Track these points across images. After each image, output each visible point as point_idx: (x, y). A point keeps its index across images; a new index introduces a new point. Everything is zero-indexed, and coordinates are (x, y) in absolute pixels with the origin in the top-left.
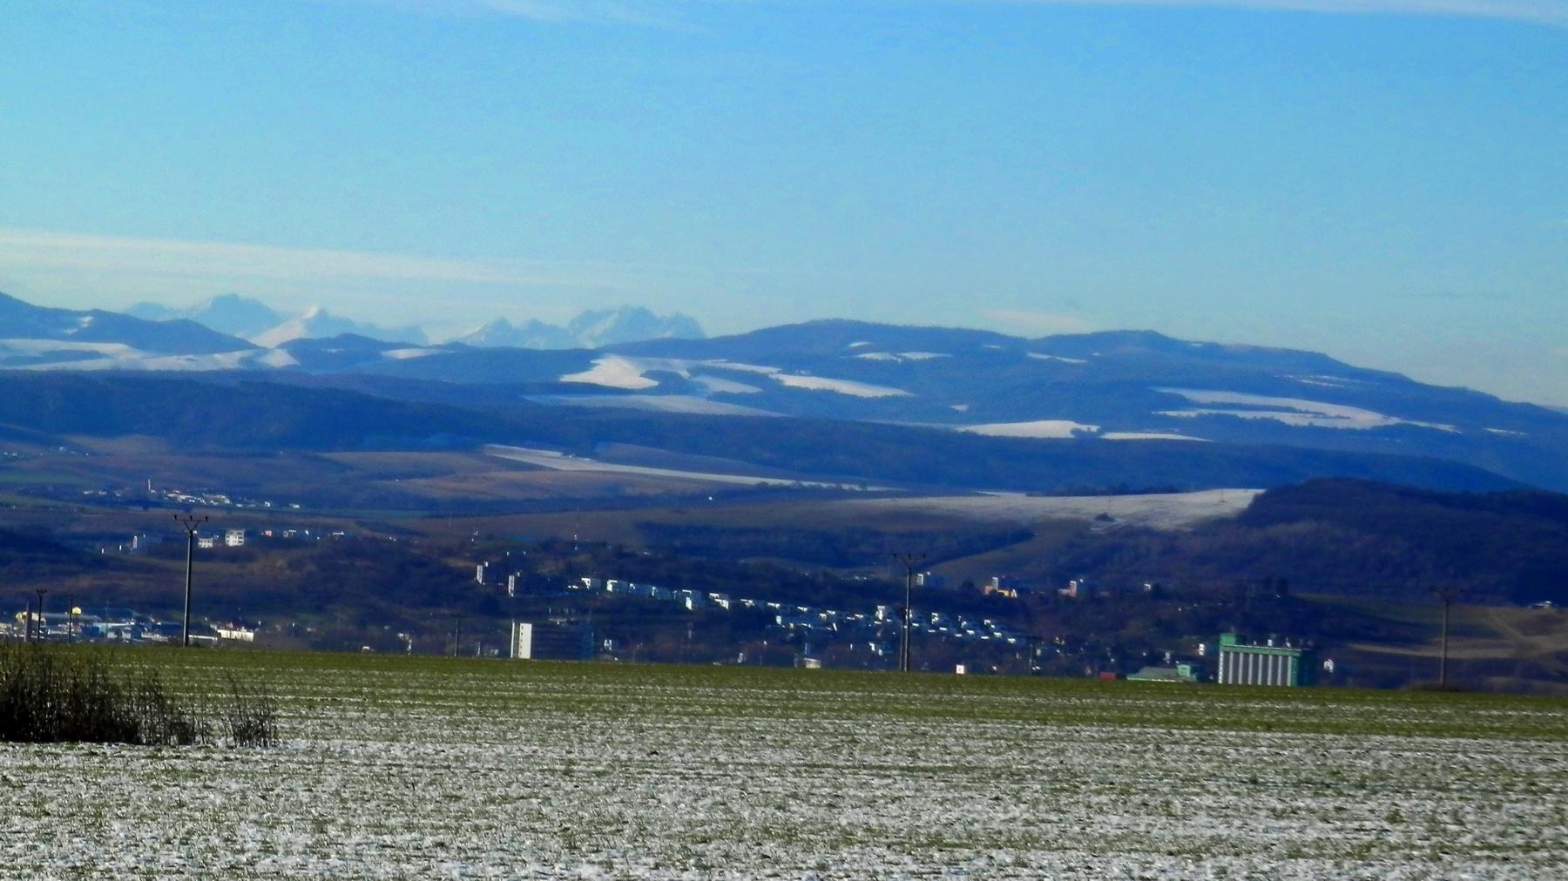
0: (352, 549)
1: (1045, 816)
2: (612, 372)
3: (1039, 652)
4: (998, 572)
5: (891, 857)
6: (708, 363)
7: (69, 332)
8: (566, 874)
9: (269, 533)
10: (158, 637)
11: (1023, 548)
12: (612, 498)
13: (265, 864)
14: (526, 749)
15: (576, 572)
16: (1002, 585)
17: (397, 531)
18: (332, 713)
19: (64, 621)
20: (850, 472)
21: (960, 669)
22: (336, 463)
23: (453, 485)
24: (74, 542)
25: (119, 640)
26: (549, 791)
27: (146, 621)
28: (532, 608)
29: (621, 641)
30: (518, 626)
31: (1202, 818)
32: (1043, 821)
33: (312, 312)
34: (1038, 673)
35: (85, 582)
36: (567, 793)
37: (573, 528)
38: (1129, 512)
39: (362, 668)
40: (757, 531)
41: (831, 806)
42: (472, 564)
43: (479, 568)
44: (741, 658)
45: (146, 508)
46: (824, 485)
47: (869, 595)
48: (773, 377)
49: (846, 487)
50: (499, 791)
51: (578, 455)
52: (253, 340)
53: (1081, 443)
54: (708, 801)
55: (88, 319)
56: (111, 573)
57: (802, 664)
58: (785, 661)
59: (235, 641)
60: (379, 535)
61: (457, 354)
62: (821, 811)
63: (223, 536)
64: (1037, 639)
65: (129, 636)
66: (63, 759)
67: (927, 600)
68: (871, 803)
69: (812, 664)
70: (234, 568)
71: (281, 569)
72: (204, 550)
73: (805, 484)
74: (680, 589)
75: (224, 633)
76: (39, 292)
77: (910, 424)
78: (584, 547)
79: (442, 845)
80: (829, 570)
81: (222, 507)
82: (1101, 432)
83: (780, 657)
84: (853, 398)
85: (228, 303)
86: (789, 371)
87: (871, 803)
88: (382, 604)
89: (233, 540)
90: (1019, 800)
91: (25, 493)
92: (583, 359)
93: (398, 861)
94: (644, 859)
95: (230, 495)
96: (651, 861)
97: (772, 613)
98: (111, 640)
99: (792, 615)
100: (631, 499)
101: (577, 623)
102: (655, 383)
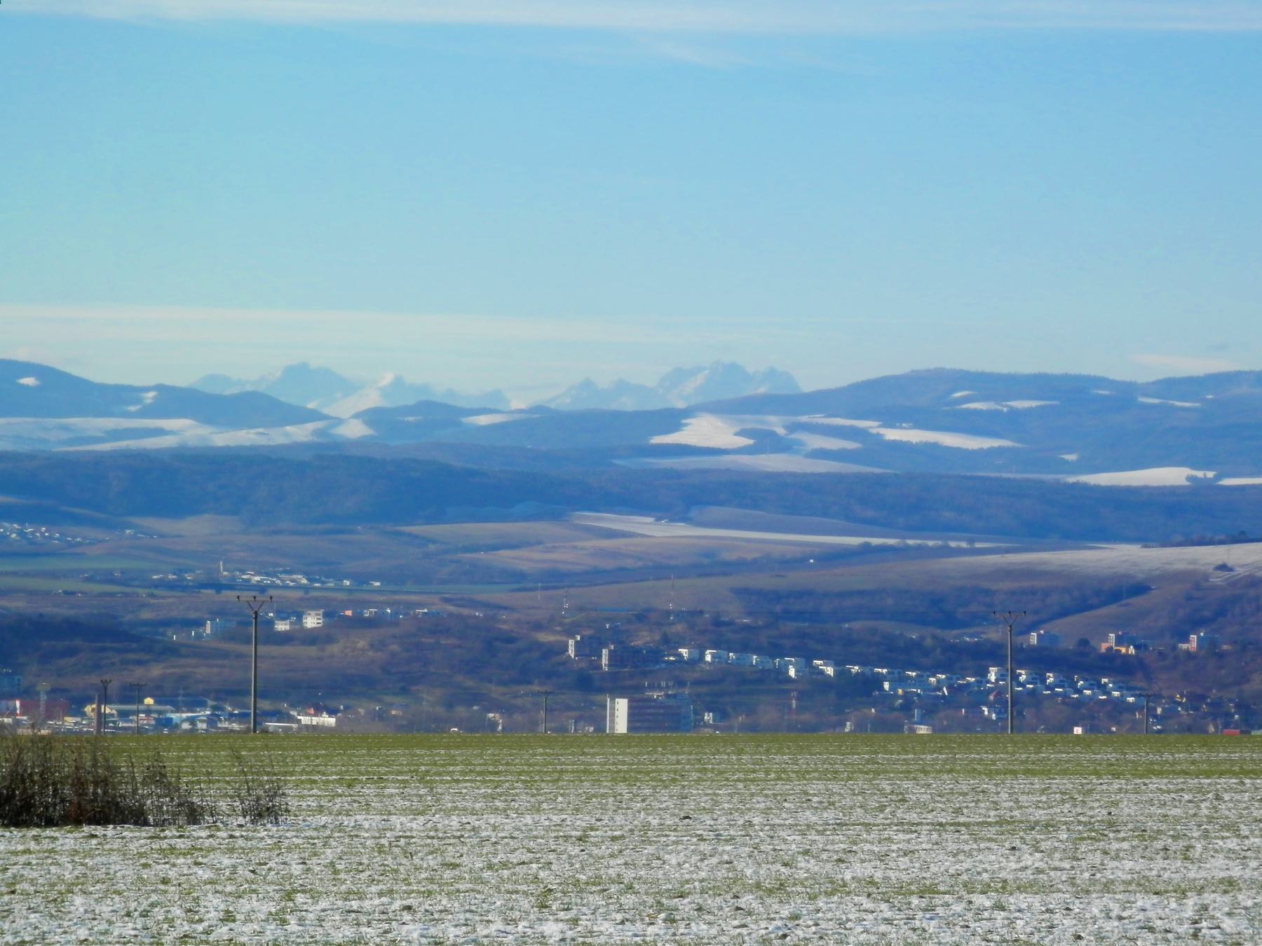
0: (437, 626)
1: (1057, 864)
2: (705, 432)
3: (1159, 711)
4: (1115, 628)
5: (867, 904)
6: (804, 419)
7: (132, 408)
8: (529, 931)
9: (349, 613)
10: (235, 726)
11: (1139, 601)
12: (708, 564)
13: (223, 932)
14: (554, 818)
15: (671, 643)
16: (1119, 641)
17: (486, 605)
18: (369, 791)
19: (137, 712)
20: (948, 529)
21: (1078, 730)
22: (416, 537)
23: (537, 556)
24: (144, 629)
25: (193, 730)
26: (552, 856)
27: (223, 709)
28: (630, 682)
29: (722, 714)
30: (613, 700)
31: (1220, 861)
32: (1056, 869)
33: (388, 378)
34: (1159, 732)
35: (156, 671)
36: (570, 857)
37: (671, 596)
38: (1249, 561)
39: (430, 748)
40: (861, 593)
41: (840, 860)
42: (564, 639)
43: (571, 642)
44: (848, 727)
45: (218, 591)
46: (931, 543)
47: (988, 654)
48: (874, 431)
49: (953, 544)
50: (501, 857)
51: (672, 520)
52: (326, 411)
53: (1197, 488)
54: (714, 860)
55: (151, 394)
56: (183, 661)
57: (912, 730)
58: (897, 728)
59: (315, 728)
60: (465, 611)
61: (542, 419)
62: (829, 866)
63: (300, 616)
64: (1157, 697)
65: (204, 726)
66: (61, 842)
67: (1040, 660)
68: (882, 857)
69: (923, 730)
70: (312, 651)
71: (363, 650)
72: (279, 632)
73: (910, 542)
74: (782, 656)
75: (305, 720)
76: (101, 370)
77: (1019, 476)
78: (678, 614)
79: (409, 908)
80: (938, 632)
81: (299, 587)
82: (1218, 478)
83: (891, 723)
84: (958, 450)
85: (298, 373)
86: (890, 425)
87: (882, 857)
88: (470, 683)
89: (312, 621)
90: (1037, 850)
91: (89, 580)
92: (673, 419)
93: (358, 925)
94: (614, 915)
95: (306, 574)
96: (619, 917)
97: (879, 680)
98: (186, 731)
99: (901, 680)
100: (727, 564)
101: (675, 696)
102: (751, 442)
